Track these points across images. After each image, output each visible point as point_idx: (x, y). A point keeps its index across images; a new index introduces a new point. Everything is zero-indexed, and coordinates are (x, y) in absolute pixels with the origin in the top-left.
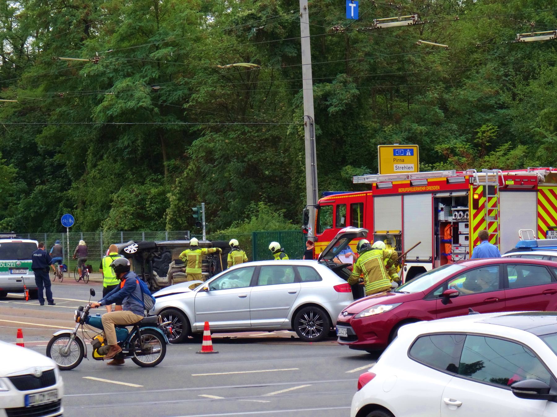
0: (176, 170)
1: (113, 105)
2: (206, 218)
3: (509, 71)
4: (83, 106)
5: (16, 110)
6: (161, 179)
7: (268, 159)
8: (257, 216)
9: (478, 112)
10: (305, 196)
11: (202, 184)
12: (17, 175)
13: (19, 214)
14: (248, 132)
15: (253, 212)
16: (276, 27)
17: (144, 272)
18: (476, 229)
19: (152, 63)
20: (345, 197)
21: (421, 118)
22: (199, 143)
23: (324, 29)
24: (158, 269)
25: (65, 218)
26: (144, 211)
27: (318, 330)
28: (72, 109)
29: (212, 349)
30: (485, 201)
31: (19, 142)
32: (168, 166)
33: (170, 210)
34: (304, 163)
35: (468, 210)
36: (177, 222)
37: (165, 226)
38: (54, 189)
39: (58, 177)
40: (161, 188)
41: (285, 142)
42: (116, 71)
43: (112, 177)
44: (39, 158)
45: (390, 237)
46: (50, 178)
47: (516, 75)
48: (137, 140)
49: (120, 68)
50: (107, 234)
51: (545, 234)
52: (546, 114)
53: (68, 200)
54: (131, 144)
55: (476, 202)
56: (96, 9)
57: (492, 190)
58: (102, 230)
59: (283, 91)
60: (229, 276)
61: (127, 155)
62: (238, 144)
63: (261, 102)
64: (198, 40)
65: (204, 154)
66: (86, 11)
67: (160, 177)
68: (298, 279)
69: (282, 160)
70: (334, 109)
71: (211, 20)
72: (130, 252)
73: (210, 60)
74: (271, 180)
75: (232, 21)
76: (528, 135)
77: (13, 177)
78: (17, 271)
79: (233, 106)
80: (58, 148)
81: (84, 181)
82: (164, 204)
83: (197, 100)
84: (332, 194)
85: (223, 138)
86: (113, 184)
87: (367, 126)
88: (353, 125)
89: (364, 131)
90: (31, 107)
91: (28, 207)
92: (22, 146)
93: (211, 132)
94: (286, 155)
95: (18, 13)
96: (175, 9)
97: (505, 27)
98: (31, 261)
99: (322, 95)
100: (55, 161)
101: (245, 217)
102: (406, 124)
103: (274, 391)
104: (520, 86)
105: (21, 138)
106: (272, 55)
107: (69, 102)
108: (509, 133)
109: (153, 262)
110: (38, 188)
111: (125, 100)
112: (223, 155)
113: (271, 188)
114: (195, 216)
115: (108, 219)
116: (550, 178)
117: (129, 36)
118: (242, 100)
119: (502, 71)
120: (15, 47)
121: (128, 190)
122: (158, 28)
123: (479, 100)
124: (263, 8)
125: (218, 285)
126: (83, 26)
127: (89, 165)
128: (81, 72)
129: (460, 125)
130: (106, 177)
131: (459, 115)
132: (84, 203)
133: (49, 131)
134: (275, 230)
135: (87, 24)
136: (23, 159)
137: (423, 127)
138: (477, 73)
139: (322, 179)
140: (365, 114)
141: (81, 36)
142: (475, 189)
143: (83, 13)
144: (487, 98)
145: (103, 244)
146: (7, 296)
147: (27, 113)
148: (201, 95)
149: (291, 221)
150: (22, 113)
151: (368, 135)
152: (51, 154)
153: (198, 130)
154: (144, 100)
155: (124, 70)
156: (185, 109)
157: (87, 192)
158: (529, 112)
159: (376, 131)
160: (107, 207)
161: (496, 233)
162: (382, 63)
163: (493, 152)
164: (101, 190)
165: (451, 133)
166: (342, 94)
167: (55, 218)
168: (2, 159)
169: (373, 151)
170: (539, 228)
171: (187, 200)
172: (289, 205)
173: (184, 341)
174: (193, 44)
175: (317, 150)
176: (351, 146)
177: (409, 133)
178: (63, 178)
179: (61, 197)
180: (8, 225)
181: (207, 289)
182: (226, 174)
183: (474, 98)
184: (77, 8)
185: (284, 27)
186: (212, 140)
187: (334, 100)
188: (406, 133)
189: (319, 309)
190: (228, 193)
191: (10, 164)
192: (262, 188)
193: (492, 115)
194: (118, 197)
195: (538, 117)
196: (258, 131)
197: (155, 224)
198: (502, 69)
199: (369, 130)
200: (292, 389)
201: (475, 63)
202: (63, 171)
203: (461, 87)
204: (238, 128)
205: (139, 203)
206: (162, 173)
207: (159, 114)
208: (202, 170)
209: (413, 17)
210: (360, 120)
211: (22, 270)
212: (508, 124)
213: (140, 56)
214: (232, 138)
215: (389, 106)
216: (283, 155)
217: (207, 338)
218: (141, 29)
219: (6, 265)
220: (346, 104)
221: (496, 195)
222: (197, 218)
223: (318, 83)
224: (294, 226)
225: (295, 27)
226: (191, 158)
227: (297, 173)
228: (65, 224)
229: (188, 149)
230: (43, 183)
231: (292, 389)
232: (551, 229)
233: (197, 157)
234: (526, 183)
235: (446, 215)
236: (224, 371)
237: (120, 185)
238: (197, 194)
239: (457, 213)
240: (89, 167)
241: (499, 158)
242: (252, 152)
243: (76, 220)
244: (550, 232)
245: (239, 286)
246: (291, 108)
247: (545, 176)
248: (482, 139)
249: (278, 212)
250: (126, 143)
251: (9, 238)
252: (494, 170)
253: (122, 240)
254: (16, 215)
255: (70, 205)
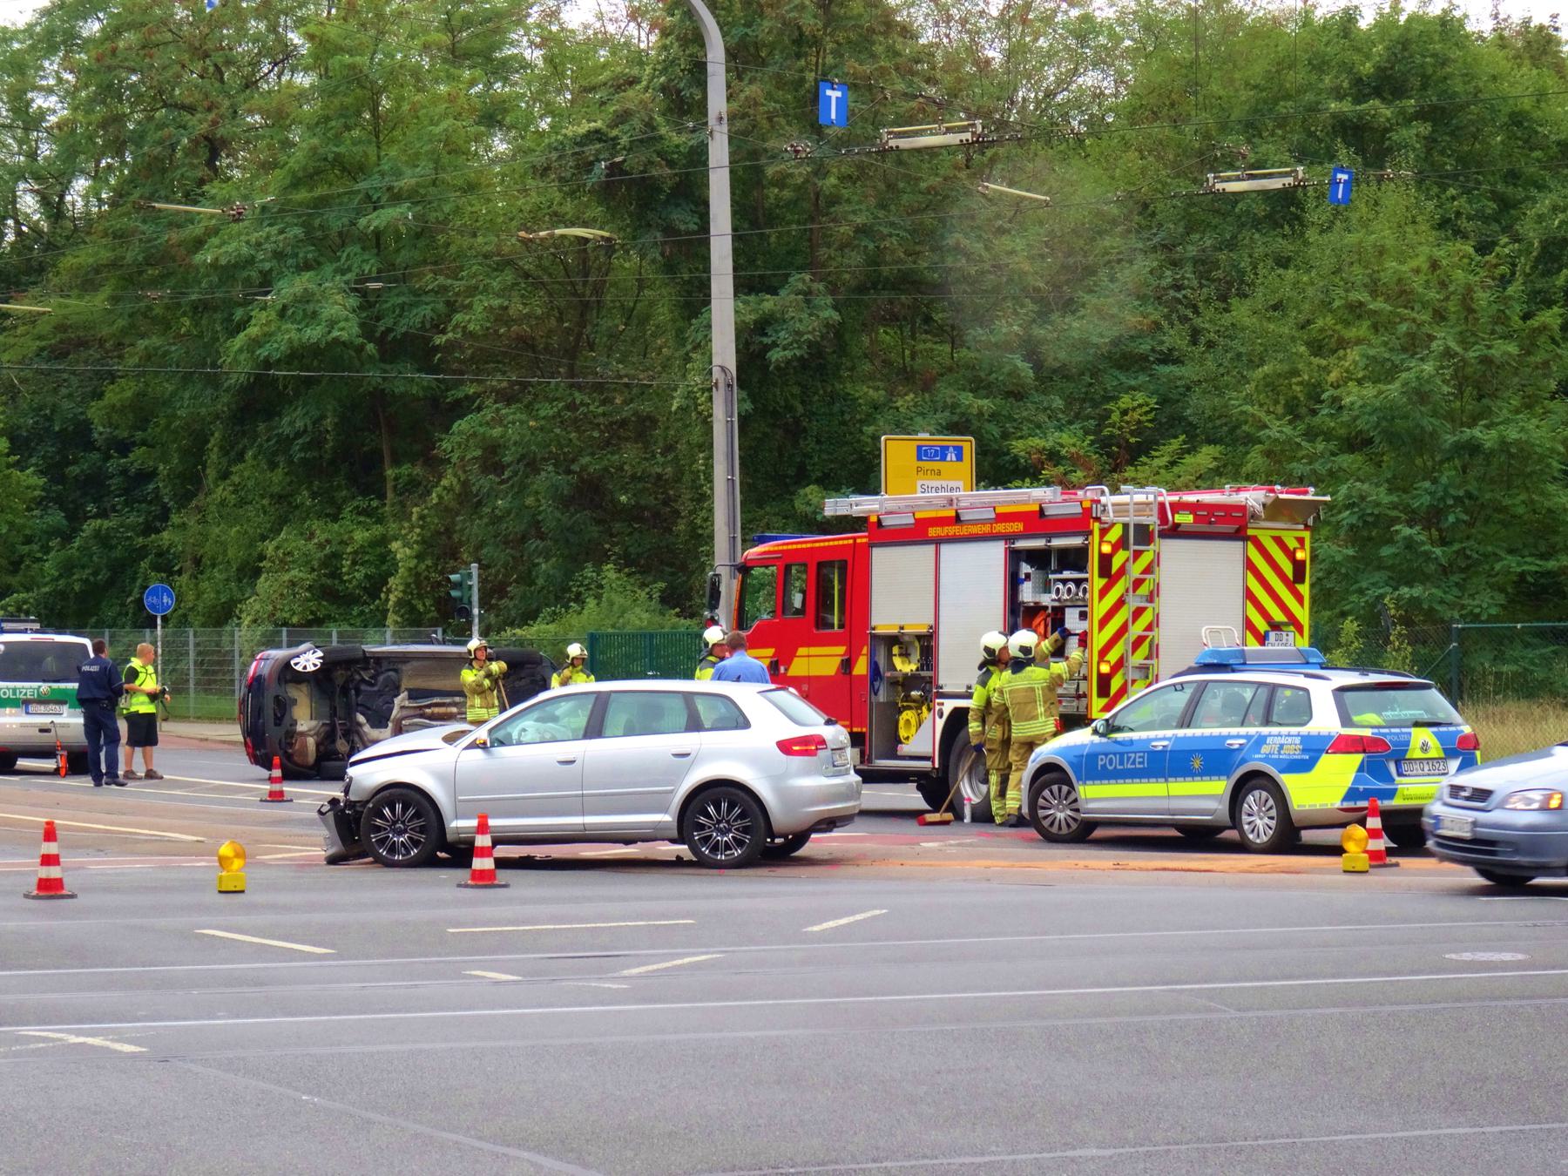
0: (413, 488)
1: (271, 335)
2: (480, 599)
3: (1183, 278)
4: (201, 336)
5: (44, 343)
6: (377, 508)
7: (626, 467)
8: (598, 597)
9: (1112, 371)
10: (711, 554)
11: (472, 521)
12: (43, 494)
13: (46, 584)
14: (582, 404)
15: (590, 589)
16: (651, 163)
17: (335, 715)
18: (1104, 622)
19: (362, 239)
20: (804, 546)
21: (982, 381)
22: (468, 427)
23: (763, 171)
24: (369, 709)
25: (155, 592)
26: (337, 582)
27: (740, 843)
28: (174, 344)
29: (495, 879)
30: (1127, 560)
31: (49, 419)
32: (396, 479)
33: (397, 581)
34: (709, 479)
35: (1086, 580)
36: (413, 609)
37: (385, 618)
38: (128, 528)
39: (140, 502)
40: (378, 530)
41: (667, 428)
42: (278, 255)
43: (265, 502)
44: (95, 456)
45: (906, 639)
46: (119, 503)
47: (1201, 286)
48: (323, 417)
49: (289, 250)
50: (249, 634)
51: (1262, 639)
52: (1266, 376)
53: (160, 555)
54: (310, 428)
55: (1106, 560)
56: (235, 112)
57: (1144, 535)
58: (239, 625)
59: (663, 313)
60: (536, 714)
61: (300, 450)
62: (558, 431)
63: (611, 336)
64: (471, 188)
65: (478, 453)
66: (211, 117)
67: (375, 504)
68: (694, 725)
69: (659, 470)
70: (782, 353)
71: (500, 146)
72: (305, 668)
73: (498, 236)
74: (633, 514)
75: (549, 145)
76: (1226, 424)
77: (34, 498)
78: (42, 708)
79: (547, 345)
80: (139, 435)
81: (199, 509)
82: (384, 568)
83: (465, 327)
84: (775, 538)
85: (524, 417)
86: (267, 518)
87: (857, 395)
88: (825, 392)
89: (848, 406)
90: (79, 338)
91: (67, 568)
92: (57, 429)
93: (496, 402)
94: (669, 458)
95: (53, 119)
96: (418, 118)
97: (1178, 176)
98: (76, 685)
99: (755, 322)
100: (132, 463)
101: (570, 600)
102: (945, 392)
103: (639, 965)
104: (1209, 313)
105: (54, 410)
106: (640, 226)
107: (168, 327)
108: (1182, 419)
109: (358, 692)
110: (90, 527)
111: (299, 323)
112: (523, 457)
113: (631, 534)
114: (454, 593)
115: (251, 600)
116: (1276, 510)
117: (311, 177)
118: (568, 331)
119: (1168, 276)
120: (45, 200)
121: (302, 534)
122: (379, 157)
123: (1116, 342)
124: (623, 117)
125: (510, 735)
126: (204, 154)
127: (211, 473)
128: (198, 258)
129: (1069, 401)
130: (251, 503)
131: (1067, 378)
132: (197, 561)
133: (116, 394)
134: (641, 628)
135: (213, 147)
136: (58, 458)
137: (986, 401)
138: (1113, 280)
139: (750, 516)
140: (852, 369)
141: (200, 174)
142: (1104, 532)
143: (206, 121)
144: (1132, 337)
145: (241, 656)
146: (16, 767)
147: (68, 353)
148: (474, 318)
149: (677, 610)
150: (59, 353)
151: (858, 417)
152: (124, 448)
153: (467, 397)
154: (342, 324)
155: (296, 255)
156: (436, 349)
157: (206, 537)
158: (1228, 373)
159: (876, 409)
160: (250, 571)
161: (1150, 634)
162: (893, 252)
163: (1144, 459)
164: (238, 532)
165: (1050, 417)
166: (801, 321)
167: (130, 595)
168: (8, 455)
169: (869, 453)
170: (1249, 625)
171: (438, 559)
172: (672, 574)
173: (428, 861)
174: (459, 197)
175: (740, 449)
176: (818, 442)
177: (952, 413)
178: (150, 502)
179: (144, 547)
180: (19, 610)
181: (485, 743)
182: (530, 501)
183: (1102, 336)
184: (191, 109)
185: (671, 164)
186: (499, 421)
187: (782, 334)
188: (947, 414)
189: (741, 794)
190: (533, 544)
191: (28, 468)
192: (612, 535)
193: (1143, 378)
194: (277, 548)
195: (1248, 383)
196: (603, 403)
197: (362, 613)
198: (1168, 273)
199: (860, 405)
200: (679, 962)
201: (1107, 258)
202: (151, 486)
203: (1073, 313)
204: (558, 395)
205: (325, 563)
206: (382, 496)
207: (377, 356)
208: (474, 489)
209: (973, 125)
210: (840, 383)
211: (52, 707)
212: (1178, 401)
213: (335, 220)
214: (544, 418)
215: (907, 352)
216: (660, 459)
217: (485, 852)
218: (338, 161)
219: (14, 693)
220: (810, 344)
221: (1152, 546)
222: (461, 599)
223: (745, 294)
224: (683, 621)
225: (698, 157)
226: (449, 461)
227: (692, 500)
228: (153, 606)
229: (442, 440)
230: (103, 514)
231: (679, 962)
232: (1275, 626)
233: (462, 459)
234: (1220, 520)
235: (1035, 591)
236: (524, 923)
237: (282, 522)
238: (461, 544)
239: (1060, 586)
240: (210, 478)
241: (1158, 473)
242: (590, 450)
243: (179, 599)
244: (1272, 635)
245: (559, 738)
246: (682, 352)
247: (1264, 505)
248: (1120, 428)
249: (647, 590)
250: (299, 424)
251: (25, 631)
252: (1148, 489)
253: (284, 644)
254: (39, 588)
255: (166, 565)
